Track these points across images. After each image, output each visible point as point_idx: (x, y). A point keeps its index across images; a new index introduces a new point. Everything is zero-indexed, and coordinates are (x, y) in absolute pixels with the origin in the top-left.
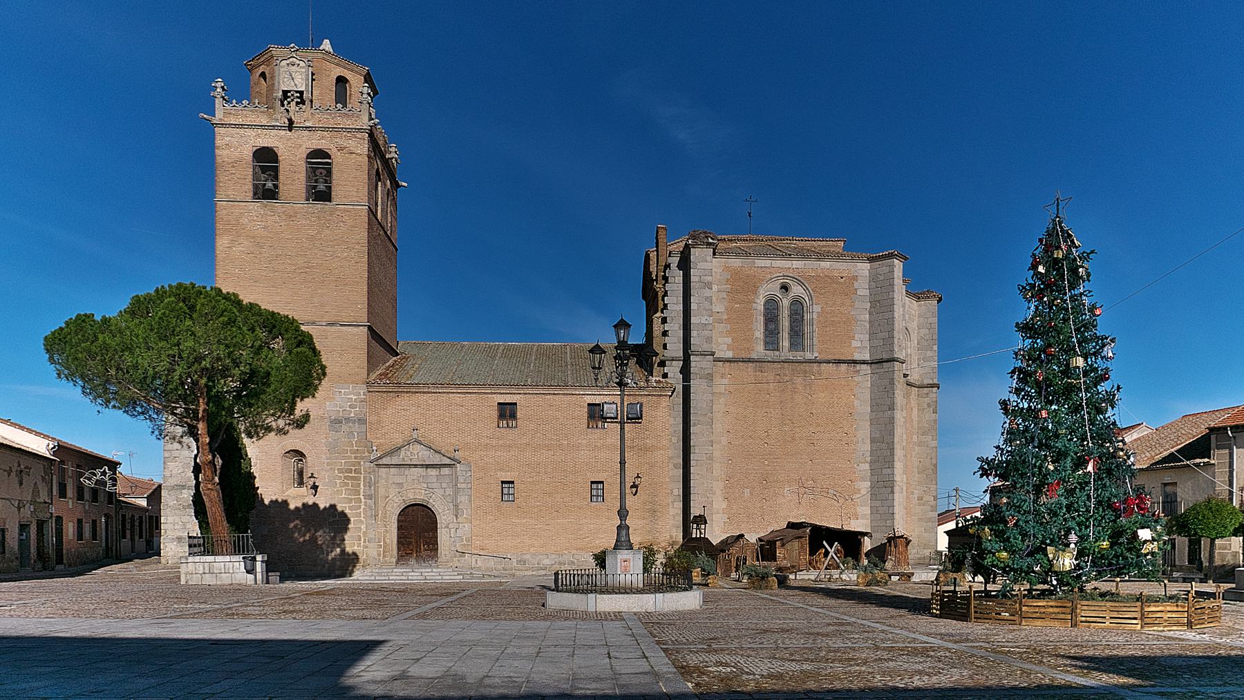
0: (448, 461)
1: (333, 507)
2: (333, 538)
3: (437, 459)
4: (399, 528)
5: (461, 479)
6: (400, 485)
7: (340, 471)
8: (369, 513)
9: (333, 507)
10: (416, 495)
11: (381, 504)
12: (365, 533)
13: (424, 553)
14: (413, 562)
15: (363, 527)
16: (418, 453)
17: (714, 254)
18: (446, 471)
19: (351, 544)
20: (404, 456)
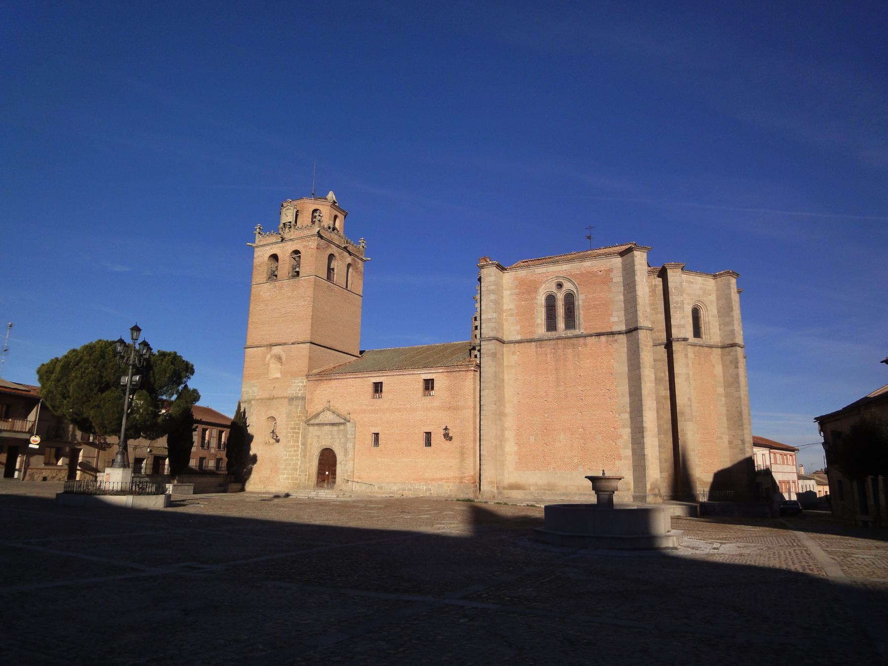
6: (318, 436)
7: (291, 429)
10: (326, 443)
16: (328, 417)
18: (342, 427)
20: (321, 419)
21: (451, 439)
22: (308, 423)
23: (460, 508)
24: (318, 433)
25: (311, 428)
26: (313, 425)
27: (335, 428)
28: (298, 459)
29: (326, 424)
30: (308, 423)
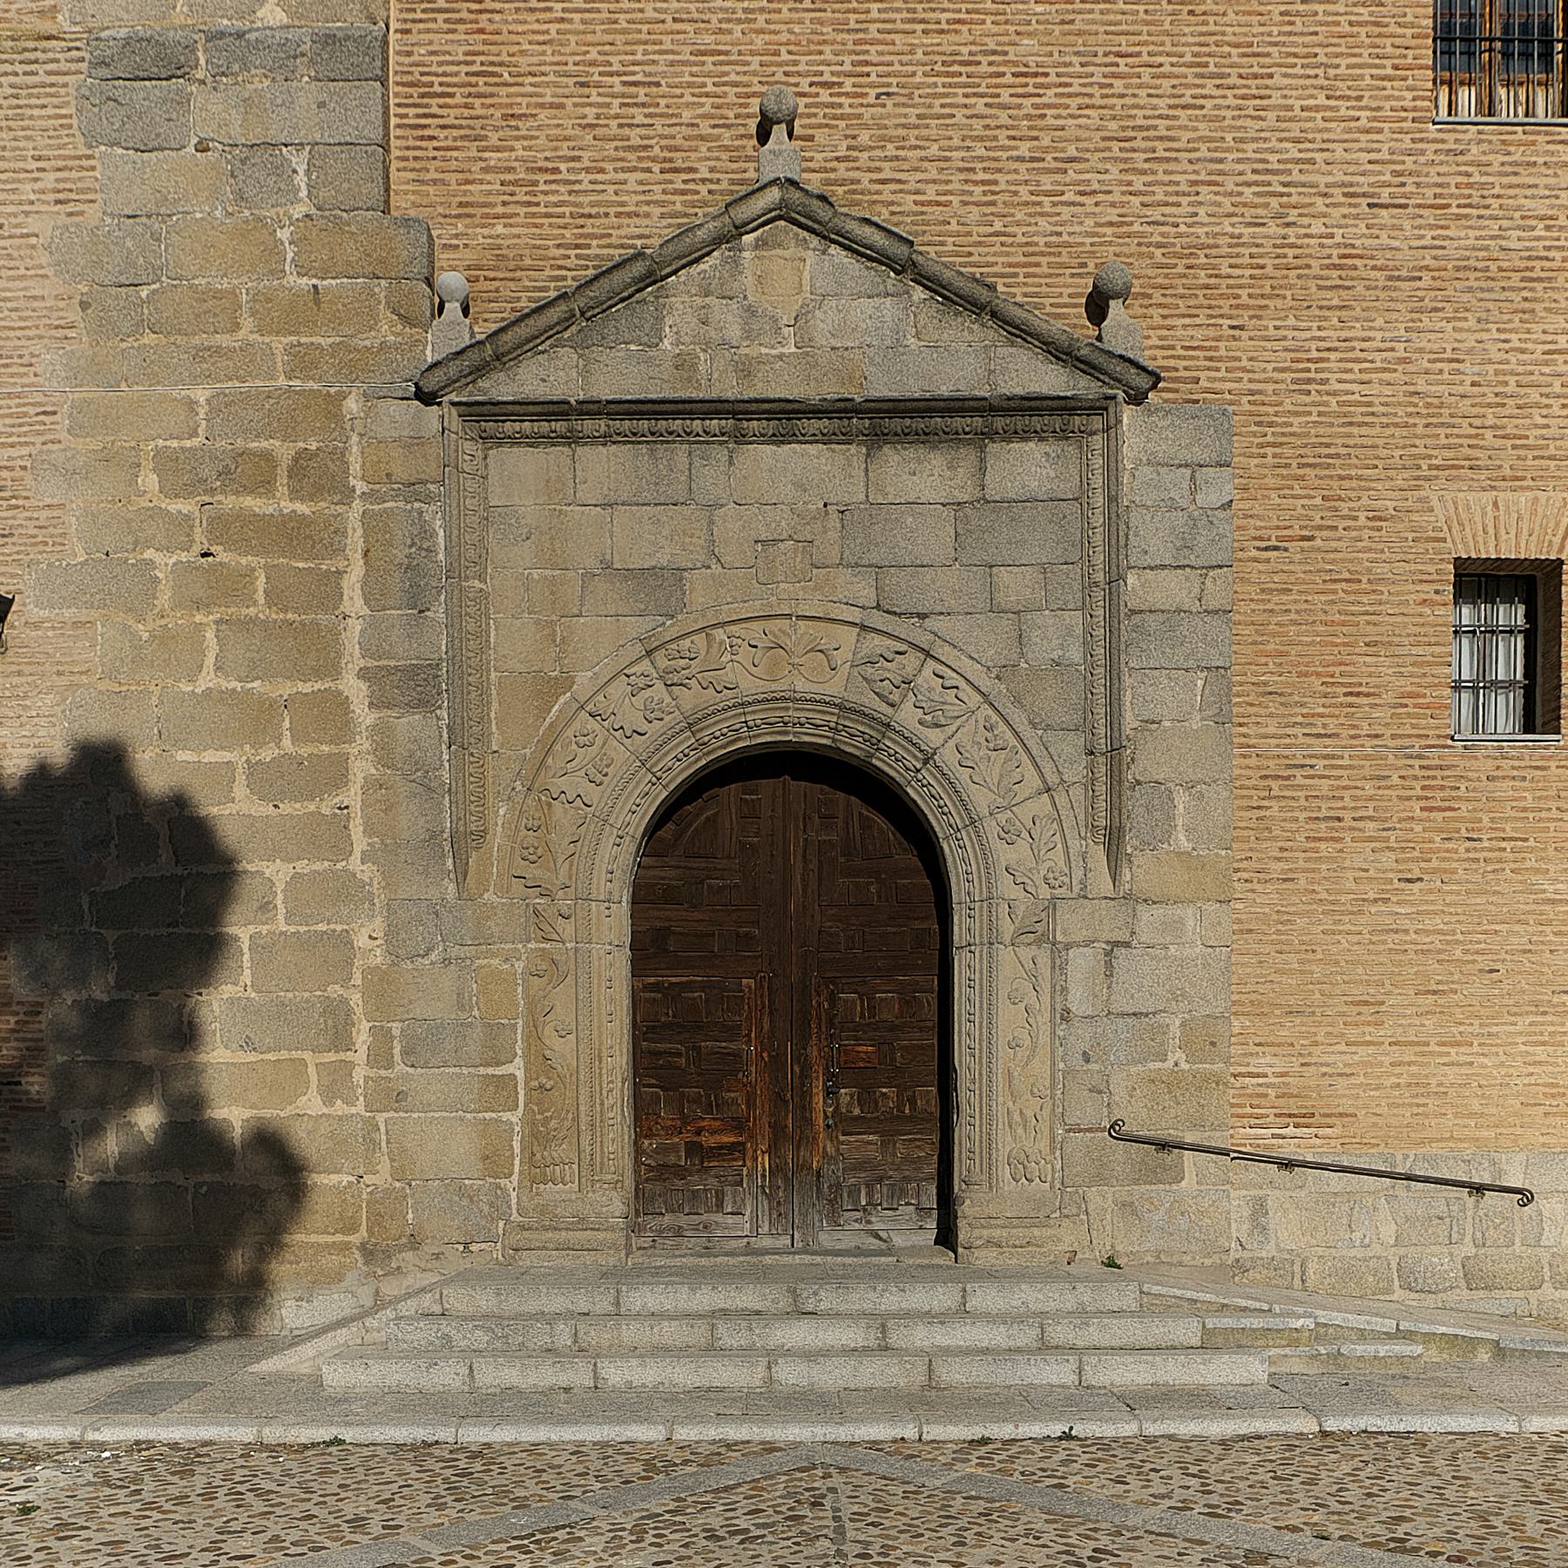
0: (1051, 380)
1: (102, 763)
2: (105, 1022)
3: (961, 361)
4: (648, 950)
5: (1151, 536)
6: (659, 585)
7: (180, 473)
8: (409, 821)
9: (102, 763)
10: (795, 671)
11: (506, 739)
12: (381, 987)
13: (832, 1151)
14: (743, 1221)
15: (367, 936)
16: (812, 318)
17: (1127, 945)
18: (1028, 466)
19: (248, 1057)
20: (691, 338)
21: (1479, 581)
22: (475, 397)
23: (984, 1258)
24: (646, 540)
25: (521, 473)
26: (561, 420)
27: (922, 477)
28: (347, 892)
29: (784, 418)
30: (475, 397)
